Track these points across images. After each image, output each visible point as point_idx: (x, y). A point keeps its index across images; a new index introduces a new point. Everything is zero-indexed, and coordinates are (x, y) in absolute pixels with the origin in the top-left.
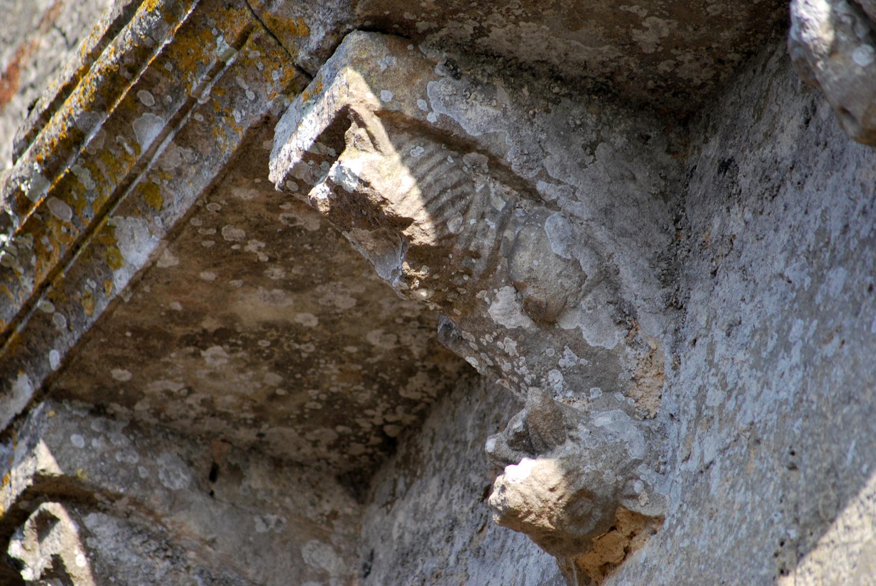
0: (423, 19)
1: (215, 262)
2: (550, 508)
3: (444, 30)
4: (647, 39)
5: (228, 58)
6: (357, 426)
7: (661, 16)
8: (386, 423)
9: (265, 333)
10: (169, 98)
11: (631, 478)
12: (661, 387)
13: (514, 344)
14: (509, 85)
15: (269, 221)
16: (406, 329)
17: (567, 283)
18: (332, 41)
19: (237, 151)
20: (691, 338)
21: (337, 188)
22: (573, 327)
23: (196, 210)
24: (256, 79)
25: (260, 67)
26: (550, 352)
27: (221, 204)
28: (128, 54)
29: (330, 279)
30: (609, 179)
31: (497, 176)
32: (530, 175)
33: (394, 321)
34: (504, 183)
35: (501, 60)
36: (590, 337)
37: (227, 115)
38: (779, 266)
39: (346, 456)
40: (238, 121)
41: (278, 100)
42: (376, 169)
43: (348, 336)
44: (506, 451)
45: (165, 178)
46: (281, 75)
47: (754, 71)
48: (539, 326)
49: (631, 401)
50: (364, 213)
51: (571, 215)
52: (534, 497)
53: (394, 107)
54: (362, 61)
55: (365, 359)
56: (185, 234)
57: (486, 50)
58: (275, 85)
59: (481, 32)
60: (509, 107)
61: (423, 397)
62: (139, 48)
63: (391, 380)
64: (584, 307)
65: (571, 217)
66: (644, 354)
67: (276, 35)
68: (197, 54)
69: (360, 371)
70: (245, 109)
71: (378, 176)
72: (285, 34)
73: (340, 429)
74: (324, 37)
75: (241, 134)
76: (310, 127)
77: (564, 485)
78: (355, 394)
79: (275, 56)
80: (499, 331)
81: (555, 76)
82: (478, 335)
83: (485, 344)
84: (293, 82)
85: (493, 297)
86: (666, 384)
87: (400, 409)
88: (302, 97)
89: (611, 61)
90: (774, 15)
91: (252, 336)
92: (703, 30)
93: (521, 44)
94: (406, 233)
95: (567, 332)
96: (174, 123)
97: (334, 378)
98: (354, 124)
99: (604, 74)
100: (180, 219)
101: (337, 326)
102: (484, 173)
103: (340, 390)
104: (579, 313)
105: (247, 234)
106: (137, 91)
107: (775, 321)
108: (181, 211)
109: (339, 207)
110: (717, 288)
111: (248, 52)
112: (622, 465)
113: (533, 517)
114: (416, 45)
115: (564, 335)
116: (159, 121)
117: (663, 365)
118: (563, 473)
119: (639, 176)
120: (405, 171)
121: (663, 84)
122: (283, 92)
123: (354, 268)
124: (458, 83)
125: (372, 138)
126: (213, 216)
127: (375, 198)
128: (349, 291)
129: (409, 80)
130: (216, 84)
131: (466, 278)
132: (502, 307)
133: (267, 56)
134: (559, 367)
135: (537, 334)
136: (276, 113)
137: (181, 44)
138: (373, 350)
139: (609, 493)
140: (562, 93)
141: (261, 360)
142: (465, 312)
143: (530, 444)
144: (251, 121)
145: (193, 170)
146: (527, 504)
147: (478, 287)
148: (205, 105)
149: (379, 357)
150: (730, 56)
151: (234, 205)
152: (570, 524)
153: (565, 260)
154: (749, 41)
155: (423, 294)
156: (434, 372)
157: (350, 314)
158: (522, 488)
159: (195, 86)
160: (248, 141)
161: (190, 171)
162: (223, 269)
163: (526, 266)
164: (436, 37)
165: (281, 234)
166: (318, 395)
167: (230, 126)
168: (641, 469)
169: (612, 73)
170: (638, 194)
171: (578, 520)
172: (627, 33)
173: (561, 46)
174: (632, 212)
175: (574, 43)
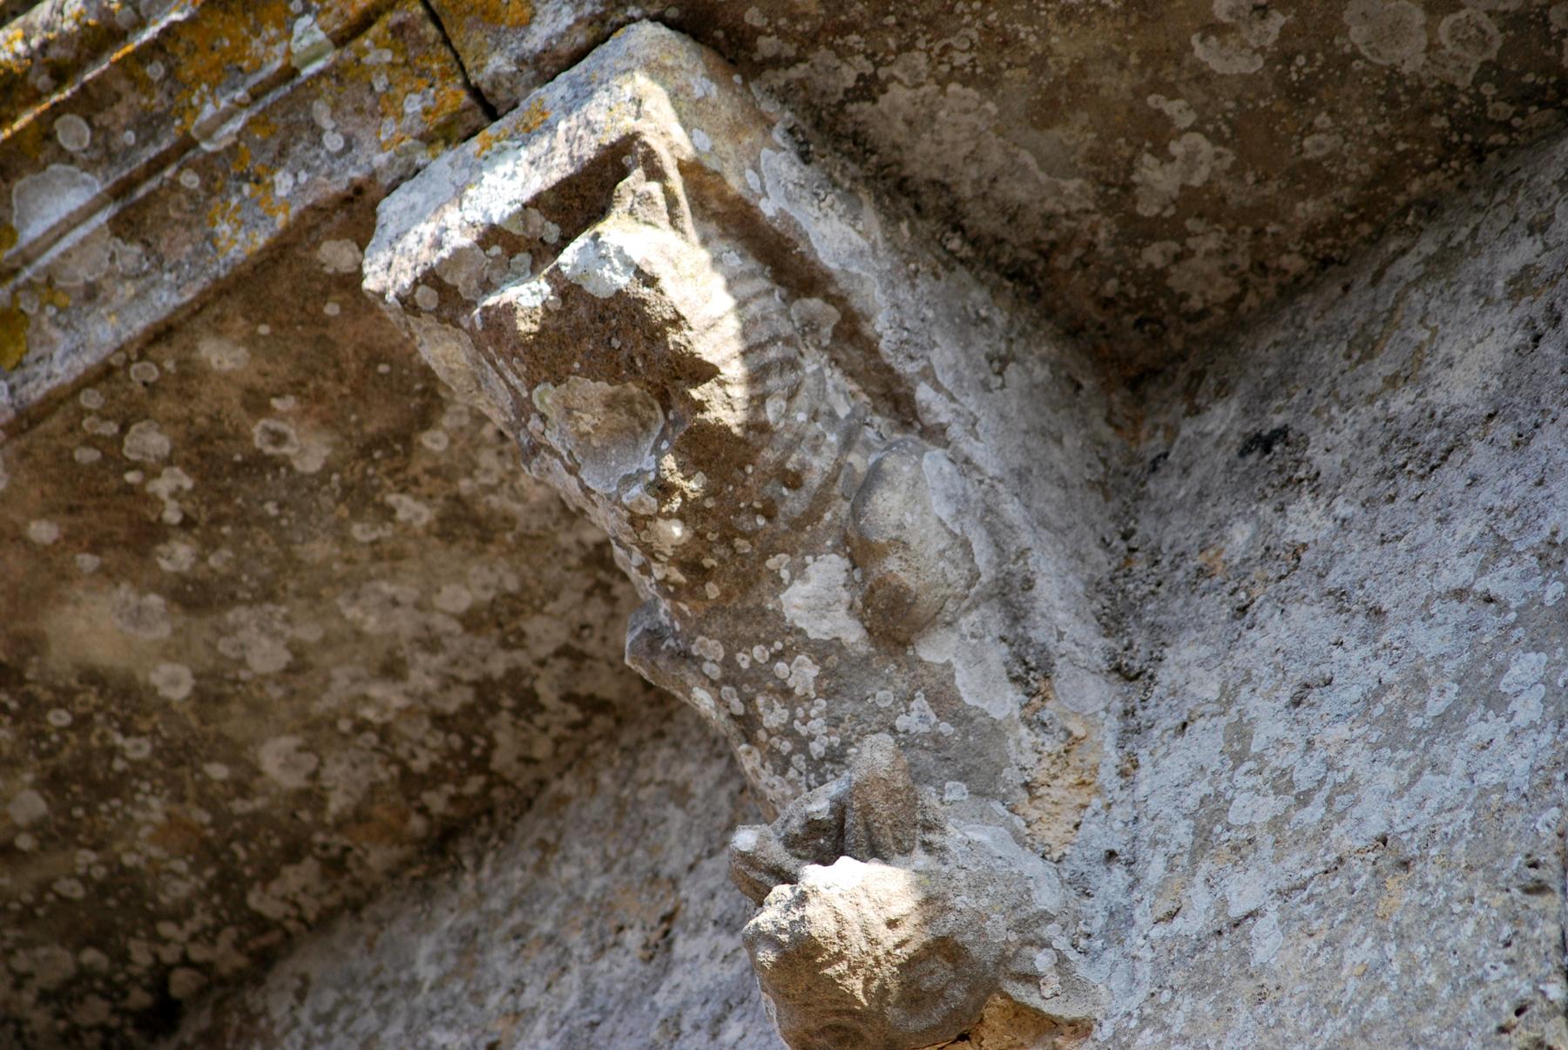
0: (778, 30)
1: (75, 502)
2: (876, 959)
3: (802, 66)
4: (1158, 181)
5: (308, 62)
6: (123, 958)
7: (1216, 138)
8: (186, 962)
9: (75, 692)
10: (129, 137)
11: (1032, 943)
12: (1084, 807)
13: (812, 671)
14: (881, 208)
15: (231, 431)
16: (345, 749)
17: (953, 575)
18: (581, 39)
19: (260, 252)
20: (1173, 721)
21: (568, 291)
22: (940, 660)
23: (105, 374)
24: (359, 111)
25: (379, 86)
26: (885, 698)
27: (161, 369)
28: (65, 39)
29: (270, 596)
30: (1024, 426)
31: (843, 357)
32: (910, 368)
33: (333, 724)
34: (850, 374)
35: (874, 159)
36: (967, 686)
37: (258, 181)
38: (1461, 572)
39: (62, 1025)
40: (281, 192)
41: (406, 151)
42: (671, 260)
43: (227, 739)
44: (777, 853)
45: (51, 302)
46: (429, 103)
47: (1346, 288)
48: (875, 644)
49: (1019, 822)
50: (616, 343)
51: (967, 461)
52: (857, 927)
53: (712, 164)
54: (664, 68)
55: (229, 799)
56: (55, 423)
57: (855, 133)
58: (406, 122)
59: (868, 88)
60: (880, 244)
61: (287, 916)
62: (95, 28)
63: (246, 863)
64: (965, 629)
65: (966, 464)
66: (1052, 745)
67: (445, 22)
68: (236, 49)
69: (203, 826)
70: (308, 168)
71: (673, 272)
72: (469, 19)
73: (90, 956)
74: (569, 28)
75: (281, 220)
76: (506, 183)
77: (915, 919)
78: (164, 878)
79: (426, 64)
80: (790, 639)
81: (954, 220)
82: (733, 643)
83: (745, 665)
84: (455, 118)
85: (799, 571)
86: (1096, 803)
87: (230, 933)
88: (474, 145)
89: (1068, 216)
90: (1416, 187)
91: (47, 696)
92: (1272, 187)
93: (926, 136)
94: (695, 394)
95: (927, 666)
96: (122, 190)
97: (145, 832)
98: (638, 173)
99: (1037, 241)
100: (61, 386)
101: (220, 710)
102: (819, 347)
103: (143, 865)
104: (955, 637)
105: (172, 451)
106: (59, 115)
107: (1449, 666)
108: (69, 370)
109: (558, 329)
110: (1254, 634)
111: (366, 51)
112: (1020, 915)
113: (842, 967)
114: (745, 80)
115: (921, 671)
116: (85, 183)
117: (1095, 769)
118: (920, 896)
119: (1067, 441)
120: (718, 281)
121: (1133, 292)
122: (421, 137)
123: (329, 581)
124: (808, 170)
125: (672, 203)
126: (131, 392)
127: (659, 311)
128: (289, 633)
129: (735, 130)
130: (263, 111)
131: (761, 521)
132: (814, 596)
133: (406, 63)
134: (893, 730)
135: (867, 659)
136: (386, 181)
137: (206, 25)
138: (257, 783)
139: (989, 957)
140: (962, 254)
141: (31, 757)
142: (727, 595)
143: (828, 840)
144: (316, 194)
145: (129, 289)
146: (842, 938)
147: (779, 544)
148: (215, 155)
149: (259, 803)
150: (1285, 260)
151: (189, 375)
152: (897, 1005)
153: (951, 532)
154: (1338, 236)
155: (677, 530)
156: (335, 866)
157: (261, 688)
158: (841, 905)
159: (208, 111)
160: (288, 239)
161: (120, 290)
162: (80, 521)
163: (894, 517)
164: (779, 78)
165: (236, 468)
166: (89, 866)
167: (258, 204)
168: (1050, 930)
169: (1053, 244)
170: (1065, 470)
171: (914, 998)
172: (1130, 161)
173: (996, 158)
174: (1057, 494)
175: (1027, 157)
